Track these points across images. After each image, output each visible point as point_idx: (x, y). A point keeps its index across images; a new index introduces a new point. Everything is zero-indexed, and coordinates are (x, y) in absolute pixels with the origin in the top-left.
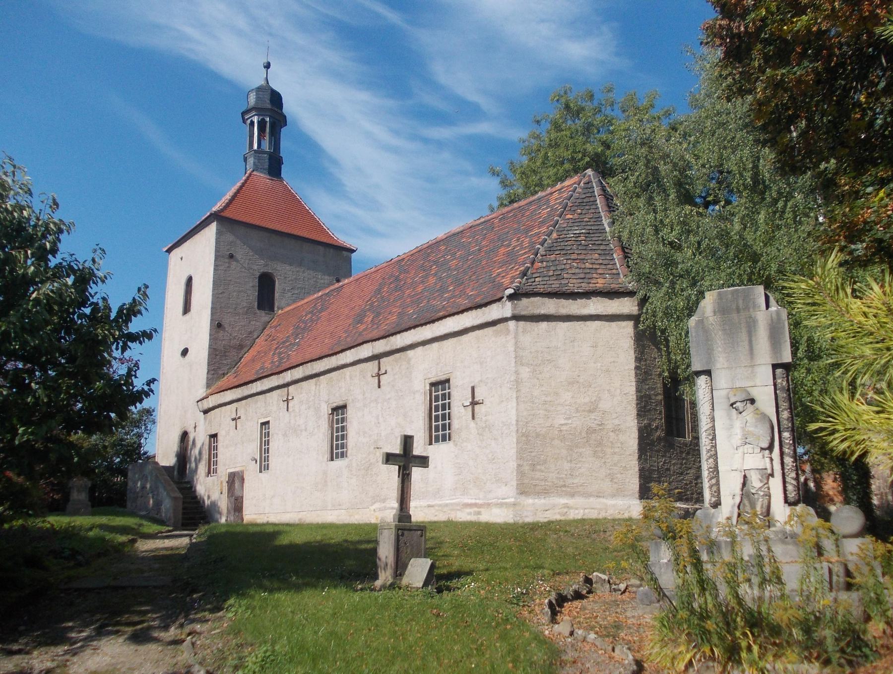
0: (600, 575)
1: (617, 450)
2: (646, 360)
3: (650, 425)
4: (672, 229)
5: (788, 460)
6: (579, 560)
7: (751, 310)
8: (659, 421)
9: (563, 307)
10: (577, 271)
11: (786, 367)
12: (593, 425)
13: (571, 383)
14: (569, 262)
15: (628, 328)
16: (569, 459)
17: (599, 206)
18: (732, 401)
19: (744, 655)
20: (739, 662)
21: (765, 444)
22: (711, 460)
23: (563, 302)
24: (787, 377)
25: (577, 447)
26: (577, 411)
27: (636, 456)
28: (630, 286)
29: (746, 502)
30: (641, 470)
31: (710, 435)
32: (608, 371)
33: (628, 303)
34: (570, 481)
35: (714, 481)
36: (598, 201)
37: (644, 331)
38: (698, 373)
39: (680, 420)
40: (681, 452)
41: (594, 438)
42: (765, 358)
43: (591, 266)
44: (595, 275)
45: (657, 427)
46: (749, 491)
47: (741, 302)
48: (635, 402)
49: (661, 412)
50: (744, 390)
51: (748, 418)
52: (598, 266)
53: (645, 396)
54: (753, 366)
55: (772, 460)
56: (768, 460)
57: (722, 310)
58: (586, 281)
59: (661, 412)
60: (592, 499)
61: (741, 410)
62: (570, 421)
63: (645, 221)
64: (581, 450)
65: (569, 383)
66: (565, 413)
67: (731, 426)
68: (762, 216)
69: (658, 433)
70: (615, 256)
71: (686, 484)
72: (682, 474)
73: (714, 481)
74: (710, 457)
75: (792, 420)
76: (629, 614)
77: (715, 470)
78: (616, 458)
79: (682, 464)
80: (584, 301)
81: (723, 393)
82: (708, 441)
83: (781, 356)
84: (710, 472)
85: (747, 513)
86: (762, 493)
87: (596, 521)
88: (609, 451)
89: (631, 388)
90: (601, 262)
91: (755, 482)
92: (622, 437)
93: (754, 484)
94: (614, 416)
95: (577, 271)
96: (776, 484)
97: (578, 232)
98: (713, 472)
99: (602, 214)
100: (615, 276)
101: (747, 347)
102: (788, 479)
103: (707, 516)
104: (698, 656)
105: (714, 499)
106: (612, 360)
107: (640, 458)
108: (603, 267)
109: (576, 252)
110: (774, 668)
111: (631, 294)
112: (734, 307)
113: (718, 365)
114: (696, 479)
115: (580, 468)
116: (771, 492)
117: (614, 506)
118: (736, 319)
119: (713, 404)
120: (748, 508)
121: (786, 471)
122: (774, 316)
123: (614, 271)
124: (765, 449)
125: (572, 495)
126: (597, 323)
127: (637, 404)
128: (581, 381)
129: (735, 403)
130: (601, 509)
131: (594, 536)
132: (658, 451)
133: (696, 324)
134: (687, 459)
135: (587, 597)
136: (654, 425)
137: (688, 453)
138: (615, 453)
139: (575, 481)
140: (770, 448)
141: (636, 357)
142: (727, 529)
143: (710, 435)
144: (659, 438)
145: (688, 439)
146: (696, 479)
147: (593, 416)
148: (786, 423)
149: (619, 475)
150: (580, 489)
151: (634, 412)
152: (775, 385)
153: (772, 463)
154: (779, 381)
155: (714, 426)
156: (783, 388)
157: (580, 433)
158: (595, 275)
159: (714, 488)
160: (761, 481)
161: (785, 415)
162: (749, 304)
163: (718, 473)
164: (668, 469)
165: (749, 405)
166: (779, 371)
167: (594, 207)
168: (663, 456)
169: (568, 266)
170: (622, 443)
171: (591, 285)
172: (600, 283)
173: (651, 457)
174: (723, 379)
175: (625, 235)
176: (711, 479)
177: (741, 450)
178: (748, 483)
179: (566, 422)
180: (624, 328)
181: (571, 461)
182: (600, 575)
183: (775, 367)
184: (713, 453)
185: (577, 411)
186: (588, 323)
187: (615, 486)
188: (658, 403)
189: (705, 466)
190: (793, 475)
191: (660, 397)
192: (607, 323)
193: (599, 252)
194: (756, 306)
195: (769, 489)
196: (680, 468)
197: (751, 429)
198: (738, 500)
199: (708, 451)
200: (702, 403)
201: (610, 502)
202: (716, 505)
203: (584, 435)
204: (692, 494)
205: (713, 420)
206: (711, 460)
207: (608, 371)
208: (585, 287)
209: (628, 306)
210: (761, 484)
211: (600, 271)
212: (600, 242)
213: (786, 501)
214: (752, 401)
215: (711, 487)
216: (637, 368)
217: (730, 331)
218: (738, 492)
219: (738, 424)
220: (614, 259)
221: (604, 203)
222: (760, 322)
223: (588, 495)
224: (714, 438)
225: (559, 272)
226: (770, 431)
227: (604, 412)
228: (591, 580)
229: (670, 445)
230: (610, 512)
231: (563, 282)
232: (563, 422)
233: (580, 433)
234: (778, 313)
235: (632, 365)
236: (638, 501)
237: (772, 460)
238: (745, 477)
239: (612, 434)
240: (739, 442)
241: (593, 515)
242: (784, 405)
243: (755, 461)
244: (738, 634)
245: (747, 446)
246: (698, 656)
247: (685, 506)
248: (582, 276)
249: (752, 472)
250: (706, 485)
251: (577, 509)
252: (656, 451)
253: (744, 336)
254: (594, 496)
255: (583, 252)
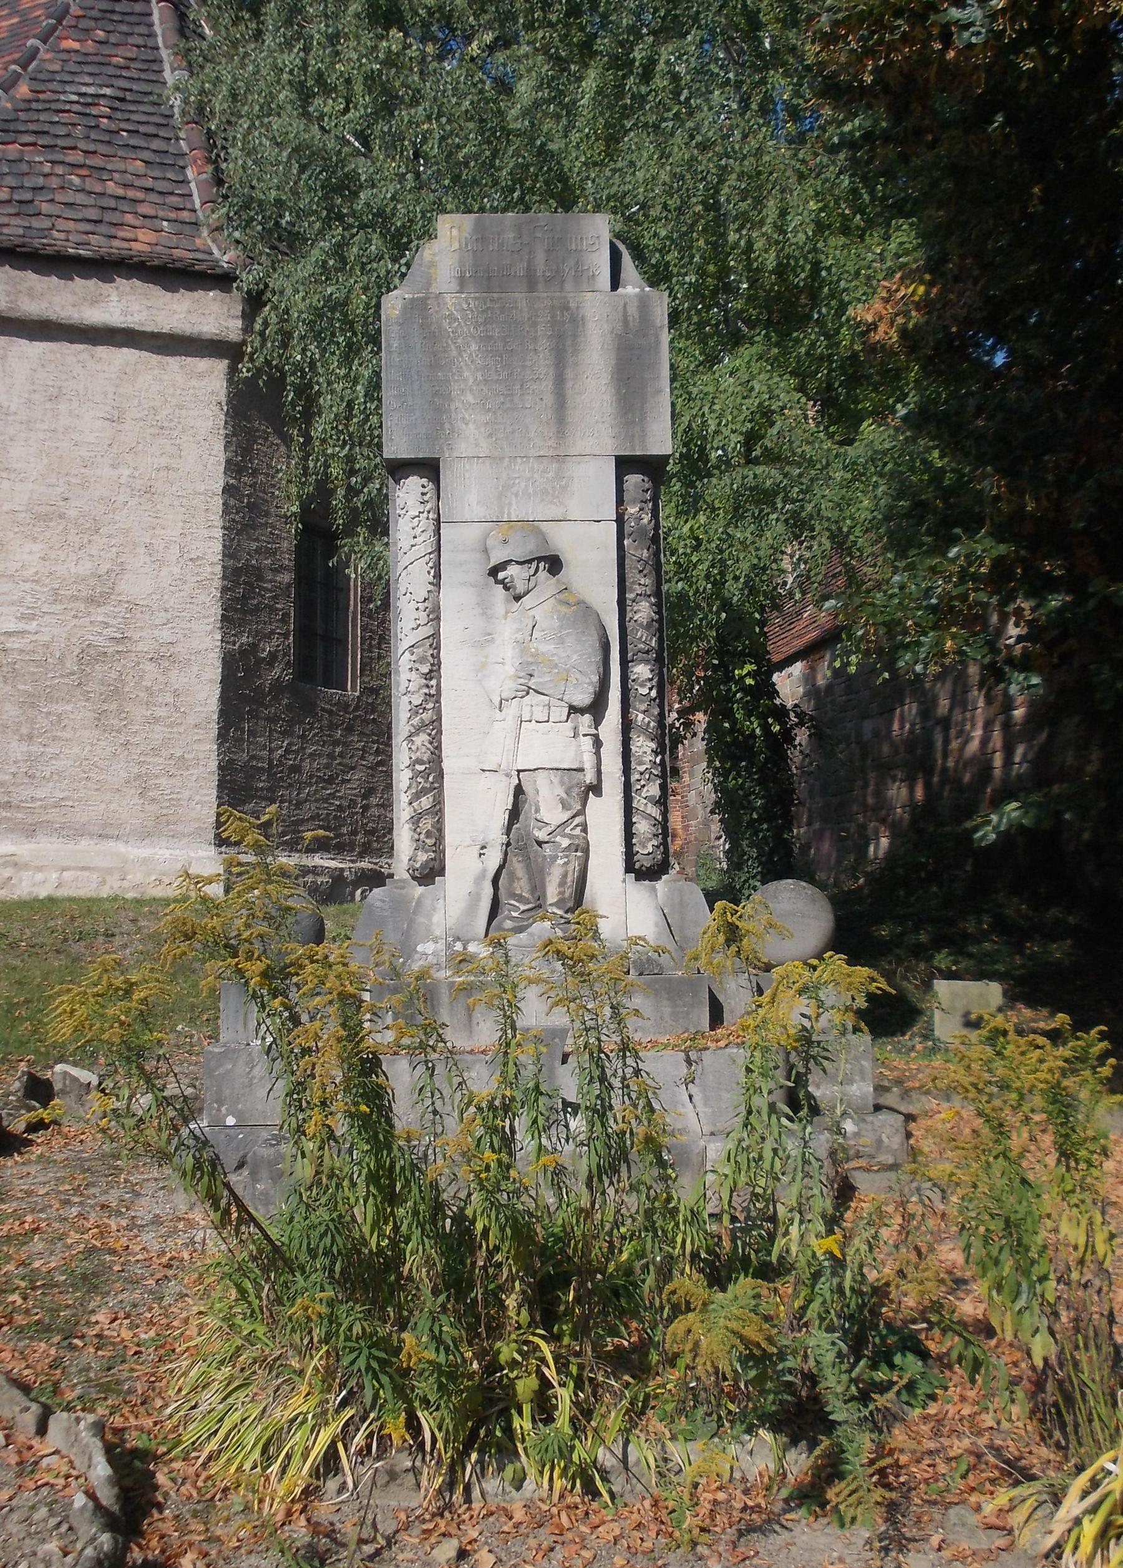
0: (75, 1072)
1: (161, 712)
2: (255, 473)
3: (254, 647)
4: (348, 101)
5: (643, 746)
6: (21, 1019)
7: (569, 286)
8: (278, 642)
9: (30, 292)
10: (80, 198)
11: (652, 467)
12: (100, 641)
13: (44, 516)
14: (59, 170)
15: (209, 379)
16: (24, 731)
17: (158, 29)
18: (493, 562)
19: (522, 1423)
20: (506, 1450)
21: (584, 698)
22: (422, 739)
23: (31, 278)
24: (655, 499)
25: (50, 698)
26: (56, 596)
27: (214, 729)
28: (226, 258)
29: (517, 866)
30: (225, 769)
31: (422, 660)
32: (149, 491)
33: (215, 307)
34: (27, 792)
35: (426, 802)
36: (156, 17)
37: (251, 382)
38: (400, 469)
39: (335, 642)
40: (332, 726)
41: (99, 674)
42: (597, 439)
43: (120, 192)
44: (129, 218)
45: (273, 656)
46: (529, 834)
47: (540, 258)
48: (217, 583)
49: (286, 615)
50: (531, 526)
51: (538, 613)
52: (140, 195)
53: (247, 569)
54: (561, 458)
55: (598, 743)
56: (587, 743)
57: (484, 276)
58: (103, 229)
59: (286, 615)
60: (85, 843)
61: (520, 588)
62: (33, 626)
63: (274, 67)
64: (59, 708)
65: (38, 517)
66: (21, 602)
67: (487, 638)
68: (590, 82)
69: (276, 672)
70: (190, 173)
71: (340, 808)
72: (330, 781)
73: (426, 802)
74: (418, 730)
75: (660, 630)
76: (144, 1209)
77: (433, 770)
78: (159, 733)
79: (331, 756)
80: (92, 284)
81: (471, 534)
82: (417, 681)
83: (643, 436)
84: (416, 774)
85: (520, 898)
86: (565, 843)
87: (89, 906)
88: (140, 713)
89: (209, 544)
90: (149, 183)
91: (548, 808)
92: (178, 679)
93: (544, 815)
94: (161, 617)
95: (80, 198)
96: (604, 817)
97: (91, 90)
98: (425, 774)
99: (164, 53)
100: (187, 229)
101: (549, 399)
102: (639, 802)
103: (399, 906)
104: (359, 1439)
105: (422, 857)
106: (164, 461)
107: (222, 736)
108: (154, 197)
109: (82, 145)
110: (625, 1460)
111: (222, 280)
112: (520, 269)
113: (463, 448)
114: (365, 796)
115: (56, 757)
116: (590, 837)
117: (145, 861)
118: (521, 312)
119: (437, 566)
120: (522, 886)
121: (635, 776)
122: (633, 310)
123: (185, 215)
124: (581, 711)
125: (30, 831)
126: (128, 355)
127: (224, 590)
128: (73, 513)
129: (503, 566)
130: (109, 871)
131: (77, 948)
132: (272, 720)
133: (405, 309)
134: (345, 744)
135: (30, 1143)
136: (267, 648)
137: (350, 730)
138: (156, 720)
139: (40, 793)
140: (597, 708)
141: (228, 462)
142: (458, 947)
143: (422, 660)
144: (278, 688)
145: (353, 692)
146: (365, 796)
147: (99, 614)
148: (643, 638)
149: (163, 781)
150: (53, 814)
151: (215, 611)
152: (620, 520)
153: (598, 754)
154: (632, 510)
155: (436, 635)
156: (641, 531)
157: (61, 660)
158: (129, 218)
159: (427, 824)
160: (565, 806)
161: (643, 611)
162: (563, 270)
163: (441, 775)
164: (296, 769)
165: (543, 574)
166: (633, 480)
167: (142, 29)
168: (284, 734)
169: (54, 182)
170: (176, 694)
171: (116, 243)
172: (142, 242)
173: (251, 733)
174: (470, 489)
175: (219, 103)
176: (417, 796)
177: (512, 709)
178: (527, 809)
179: (21, 626)
180: (201, 376)
181: (30, 737)
182: (75, 1072)
183: (625, 465)
184: (427, 716)
185: (56, 596)
186: (102, 351)
187: (154, 807)
188: (281, 591)
189: (402, 757)
190: (654, 790)
191: (287, 578)
192: (155, 359)
193: (147, 155)
194: (582, 276)
195: (585, 828)
196: (327, 766)
197: (544, 648)
198: (494, 859)
199: (415, 711)
200: (404, 561)
201: (135, 851)
202: (430, 873)
203: (71, 664)
204: (354, 833)
205: (435, 615)
206: (422, 739)
207: (149, 491)
208: (98, 244)
209: (212, 314)
210: (567, 815)
211: (144, 209)
212: (151, 130)
213: (629, 867)
214: (554, 564)
215: (416, 820)
216: (228, 490)
217: (504, 347)
218: (497, 836)
219: (508, 630)
220: (185, 182)
221: (172, 24)
222: (591, 325)
223: (75, 832)
224: (434, 672)
225: (28, 196)
226: (598, 657)
227: (133, 606)
228: (48, 1085)
229: (307, 707)
230: (135, 877)
231: (36, 223)
232: (12, 626)
233: (61, 660)
234: (644, 304)
235: (218, 483)
236: (212, 851)
237: (598, 743)
238: (519, 791)
239: (149, 667)
240: (509, 687)
241: (84, 886)
242: (640, 583)
243: (553, 744)
244: (507, 1351)
245: (533, 698)
246: (359, 1439)
247: (333, 864)
248: (93, 214)
249: (542, 779)
250: (403, 811)
251: (40, 869)
252: (269, 719)
253: (542, 363)
254: (91, 835)
255: (102, 149)
